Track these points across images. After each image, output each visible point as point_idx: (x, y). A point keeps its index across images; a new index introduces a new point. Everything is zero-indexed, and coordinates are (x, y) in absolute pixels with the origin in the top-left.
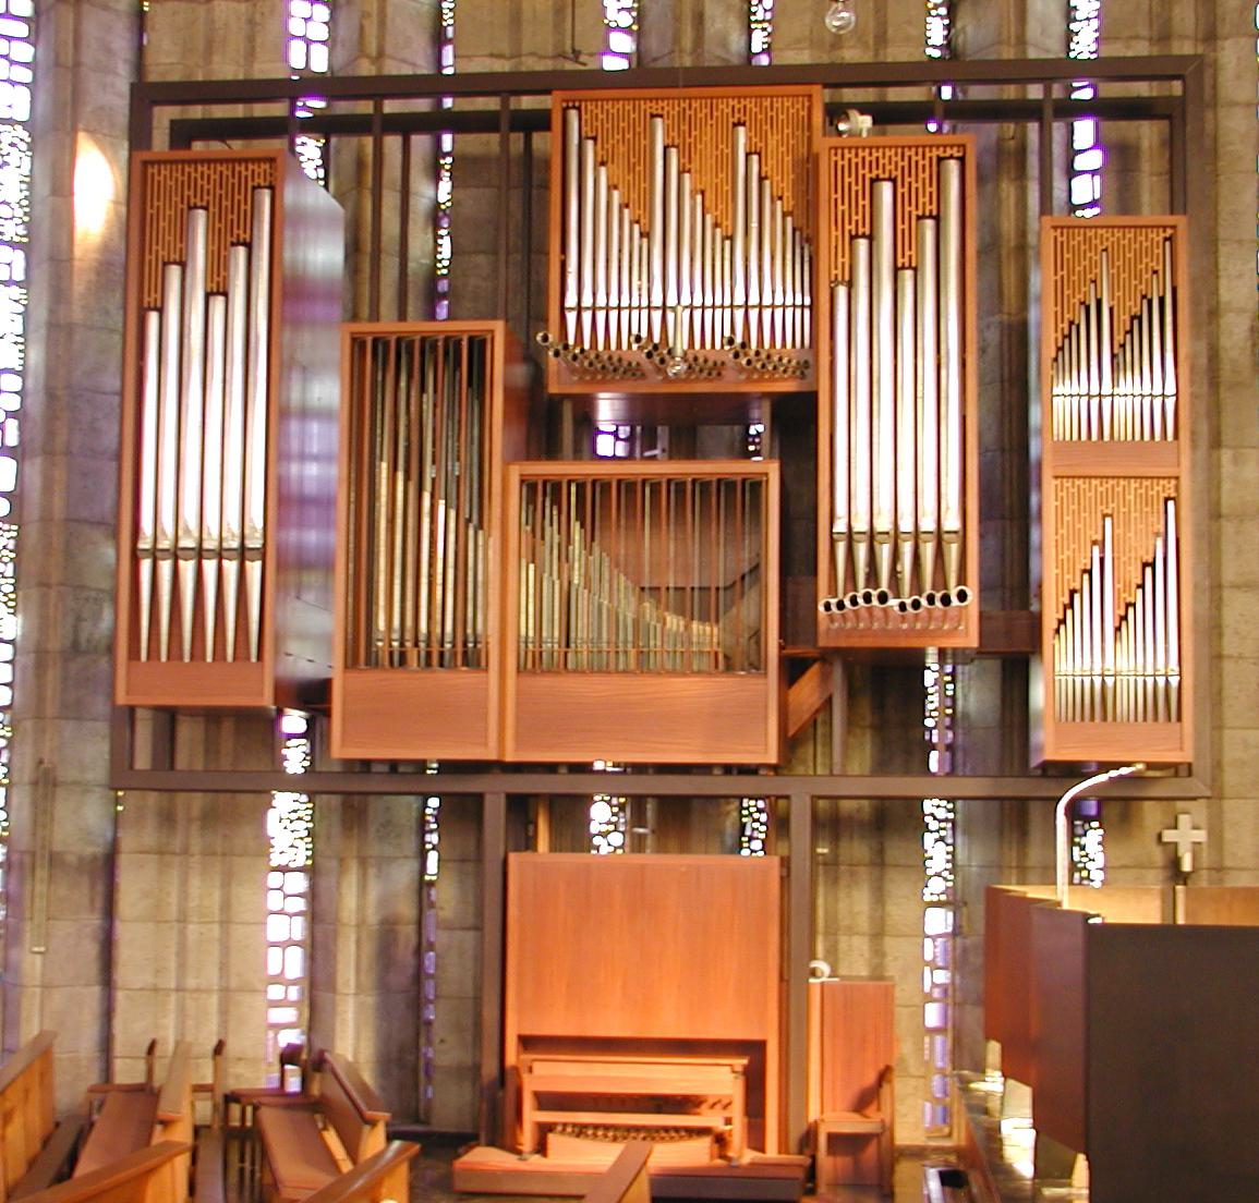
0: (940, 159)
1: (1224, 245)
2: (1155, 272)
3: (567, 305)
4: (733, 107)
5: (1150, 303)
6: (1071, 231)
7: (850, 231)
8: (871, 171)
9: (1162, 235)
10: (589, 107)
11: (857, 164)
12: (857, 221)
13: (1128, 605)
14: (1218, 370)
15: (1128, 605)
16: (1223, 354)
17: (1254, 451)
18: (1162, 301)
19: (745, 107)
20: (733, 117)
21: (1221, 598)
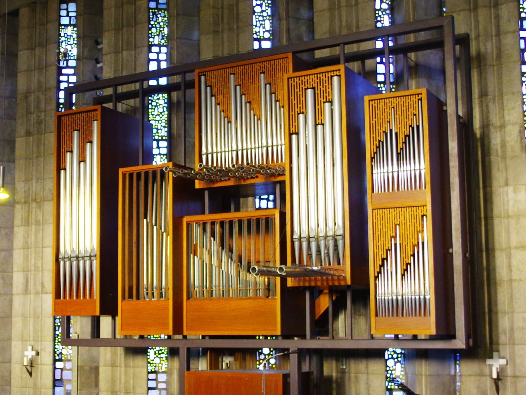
0: (332, 76)
1: (506, 95)
2: (415, 115)
3: (202, 153)
4: (260, 66)
5: (413, 128)
6: (378, 101)
7: (298, 112)
8: (305, 86)
9: (417, 98)
10: (209, 74)
11: (299, 83)
12: (300, 107)
14: (506, 151)
15: (407, 264)
16: (507, 144)
17: (524, 186)
18: (418, 127)
19: (265, 65)
20: (260, 70)
21: (510, 254)
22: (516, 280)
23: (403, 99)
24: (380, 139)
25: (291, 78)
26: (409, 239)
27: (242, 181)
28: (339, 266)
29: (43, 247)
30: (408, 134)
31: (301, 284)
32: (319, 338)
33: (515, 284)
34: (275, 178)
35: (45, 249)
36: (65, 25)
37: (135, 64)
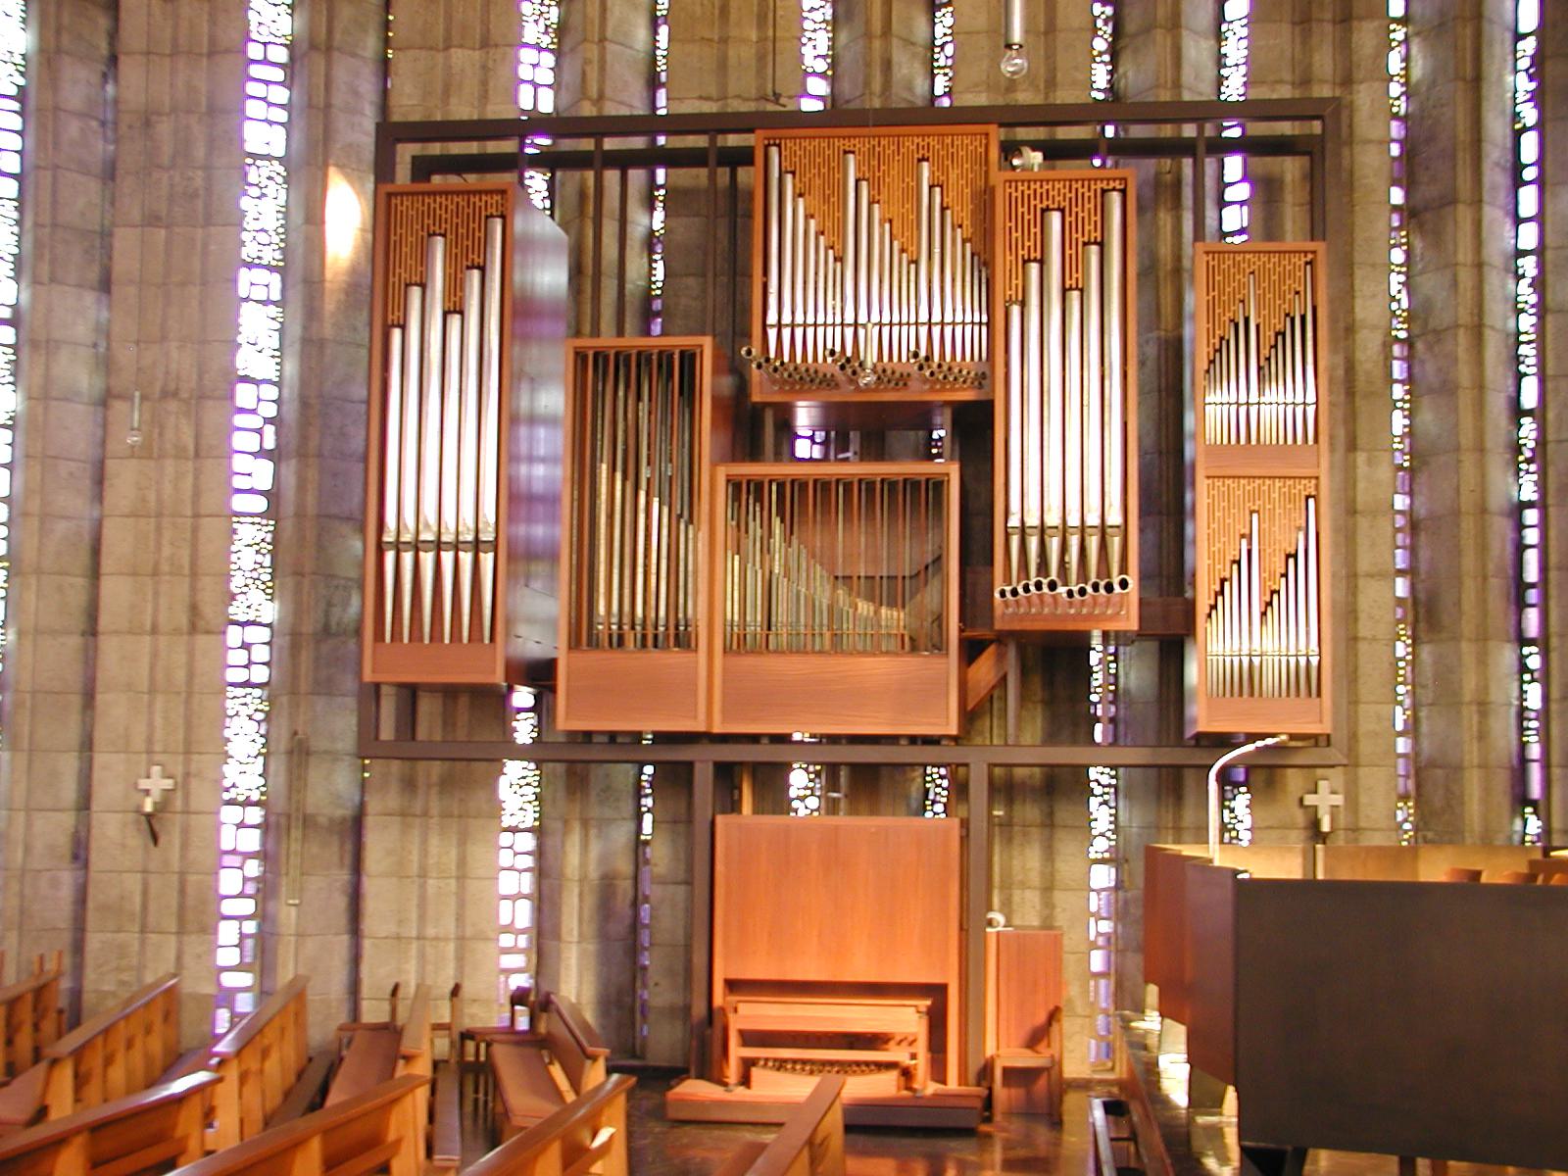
0: (1104, 192)
2: (1297, 293)
5: (1293, 320)
8: (1041, 202)
9: (1303, 260)
11: (1029, 196)
12: (1029, 247)
14: (1354, 381)
15: (1273, 592)
18: (1303, 318)
21: (1356, 586)
22: (1365, 639)
23: (1275, 259)
25: (1010, 182)
29: (196, 516)
33: (1363, 647)
35: (205, 521)
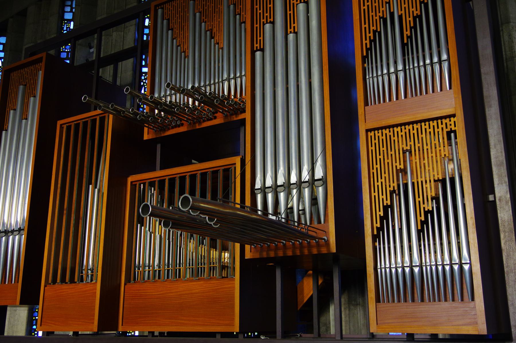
13: (426, 213)
24: (375, 29)
26: (427, 171)
27: (197, 125)
28: (319, 225)
30: (419, 14)
31: (265, 255)
32: (301, 336)
34: (236, 117)
36: (67, 20)
37: (123, 43)
